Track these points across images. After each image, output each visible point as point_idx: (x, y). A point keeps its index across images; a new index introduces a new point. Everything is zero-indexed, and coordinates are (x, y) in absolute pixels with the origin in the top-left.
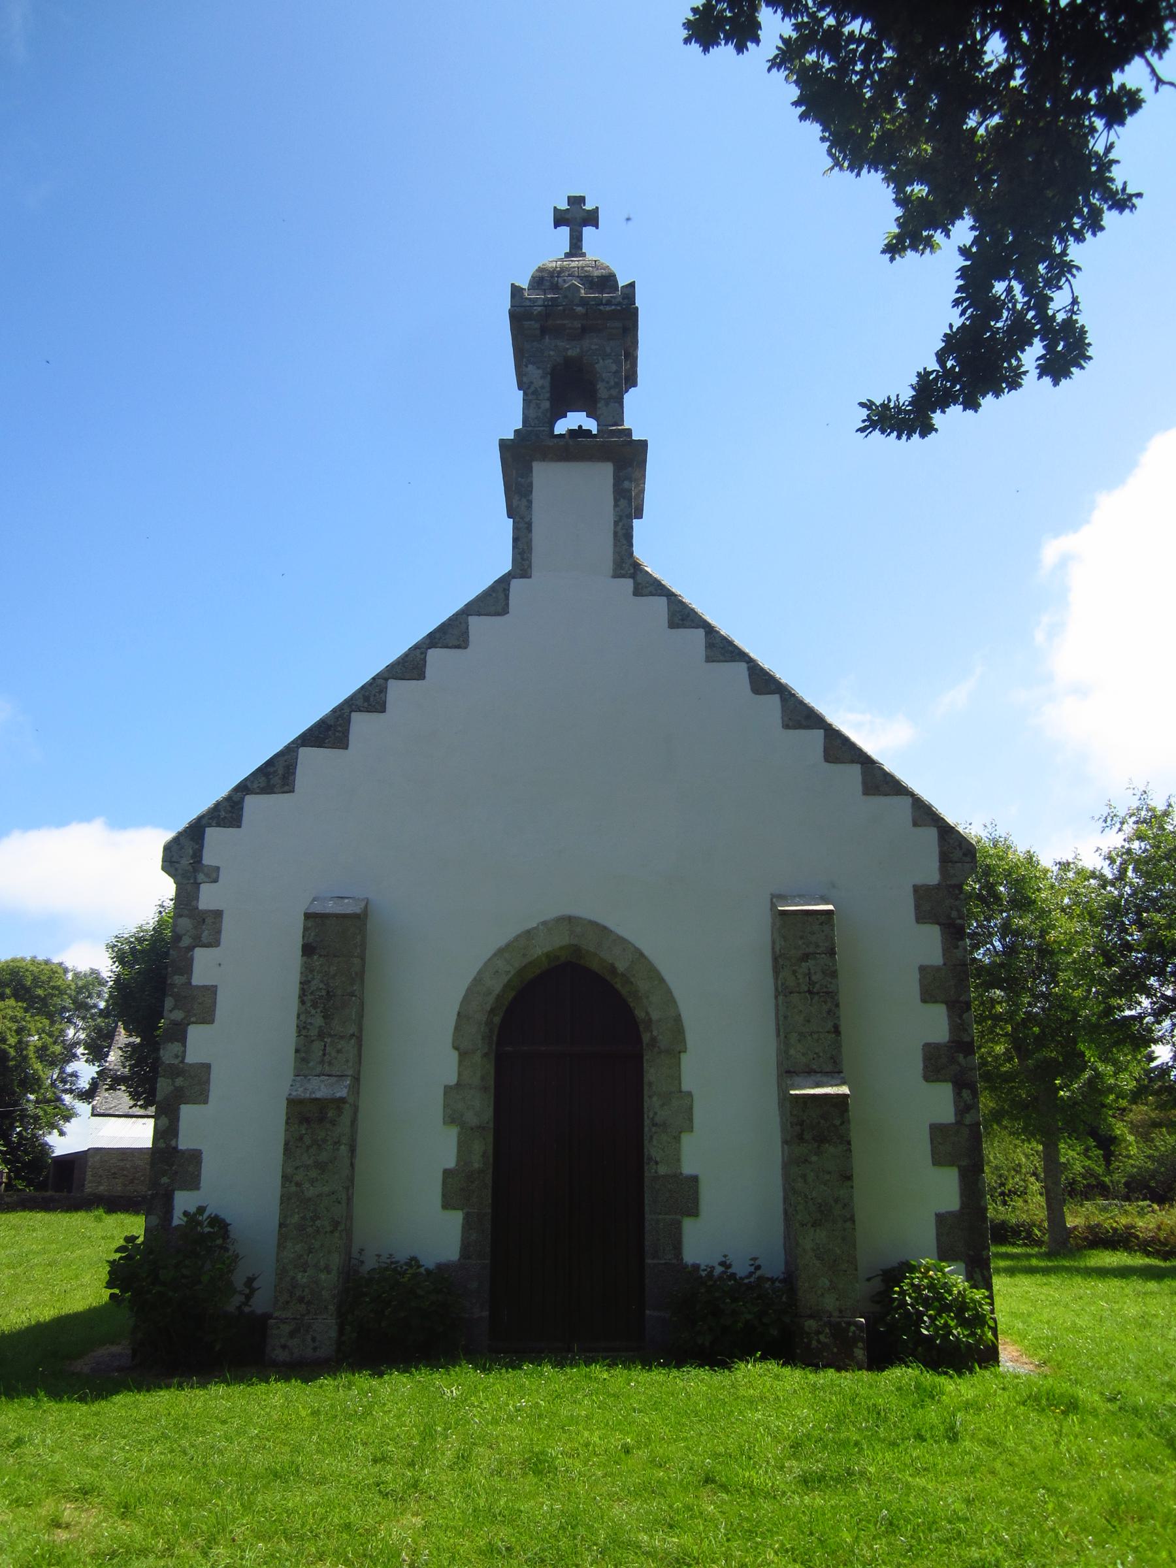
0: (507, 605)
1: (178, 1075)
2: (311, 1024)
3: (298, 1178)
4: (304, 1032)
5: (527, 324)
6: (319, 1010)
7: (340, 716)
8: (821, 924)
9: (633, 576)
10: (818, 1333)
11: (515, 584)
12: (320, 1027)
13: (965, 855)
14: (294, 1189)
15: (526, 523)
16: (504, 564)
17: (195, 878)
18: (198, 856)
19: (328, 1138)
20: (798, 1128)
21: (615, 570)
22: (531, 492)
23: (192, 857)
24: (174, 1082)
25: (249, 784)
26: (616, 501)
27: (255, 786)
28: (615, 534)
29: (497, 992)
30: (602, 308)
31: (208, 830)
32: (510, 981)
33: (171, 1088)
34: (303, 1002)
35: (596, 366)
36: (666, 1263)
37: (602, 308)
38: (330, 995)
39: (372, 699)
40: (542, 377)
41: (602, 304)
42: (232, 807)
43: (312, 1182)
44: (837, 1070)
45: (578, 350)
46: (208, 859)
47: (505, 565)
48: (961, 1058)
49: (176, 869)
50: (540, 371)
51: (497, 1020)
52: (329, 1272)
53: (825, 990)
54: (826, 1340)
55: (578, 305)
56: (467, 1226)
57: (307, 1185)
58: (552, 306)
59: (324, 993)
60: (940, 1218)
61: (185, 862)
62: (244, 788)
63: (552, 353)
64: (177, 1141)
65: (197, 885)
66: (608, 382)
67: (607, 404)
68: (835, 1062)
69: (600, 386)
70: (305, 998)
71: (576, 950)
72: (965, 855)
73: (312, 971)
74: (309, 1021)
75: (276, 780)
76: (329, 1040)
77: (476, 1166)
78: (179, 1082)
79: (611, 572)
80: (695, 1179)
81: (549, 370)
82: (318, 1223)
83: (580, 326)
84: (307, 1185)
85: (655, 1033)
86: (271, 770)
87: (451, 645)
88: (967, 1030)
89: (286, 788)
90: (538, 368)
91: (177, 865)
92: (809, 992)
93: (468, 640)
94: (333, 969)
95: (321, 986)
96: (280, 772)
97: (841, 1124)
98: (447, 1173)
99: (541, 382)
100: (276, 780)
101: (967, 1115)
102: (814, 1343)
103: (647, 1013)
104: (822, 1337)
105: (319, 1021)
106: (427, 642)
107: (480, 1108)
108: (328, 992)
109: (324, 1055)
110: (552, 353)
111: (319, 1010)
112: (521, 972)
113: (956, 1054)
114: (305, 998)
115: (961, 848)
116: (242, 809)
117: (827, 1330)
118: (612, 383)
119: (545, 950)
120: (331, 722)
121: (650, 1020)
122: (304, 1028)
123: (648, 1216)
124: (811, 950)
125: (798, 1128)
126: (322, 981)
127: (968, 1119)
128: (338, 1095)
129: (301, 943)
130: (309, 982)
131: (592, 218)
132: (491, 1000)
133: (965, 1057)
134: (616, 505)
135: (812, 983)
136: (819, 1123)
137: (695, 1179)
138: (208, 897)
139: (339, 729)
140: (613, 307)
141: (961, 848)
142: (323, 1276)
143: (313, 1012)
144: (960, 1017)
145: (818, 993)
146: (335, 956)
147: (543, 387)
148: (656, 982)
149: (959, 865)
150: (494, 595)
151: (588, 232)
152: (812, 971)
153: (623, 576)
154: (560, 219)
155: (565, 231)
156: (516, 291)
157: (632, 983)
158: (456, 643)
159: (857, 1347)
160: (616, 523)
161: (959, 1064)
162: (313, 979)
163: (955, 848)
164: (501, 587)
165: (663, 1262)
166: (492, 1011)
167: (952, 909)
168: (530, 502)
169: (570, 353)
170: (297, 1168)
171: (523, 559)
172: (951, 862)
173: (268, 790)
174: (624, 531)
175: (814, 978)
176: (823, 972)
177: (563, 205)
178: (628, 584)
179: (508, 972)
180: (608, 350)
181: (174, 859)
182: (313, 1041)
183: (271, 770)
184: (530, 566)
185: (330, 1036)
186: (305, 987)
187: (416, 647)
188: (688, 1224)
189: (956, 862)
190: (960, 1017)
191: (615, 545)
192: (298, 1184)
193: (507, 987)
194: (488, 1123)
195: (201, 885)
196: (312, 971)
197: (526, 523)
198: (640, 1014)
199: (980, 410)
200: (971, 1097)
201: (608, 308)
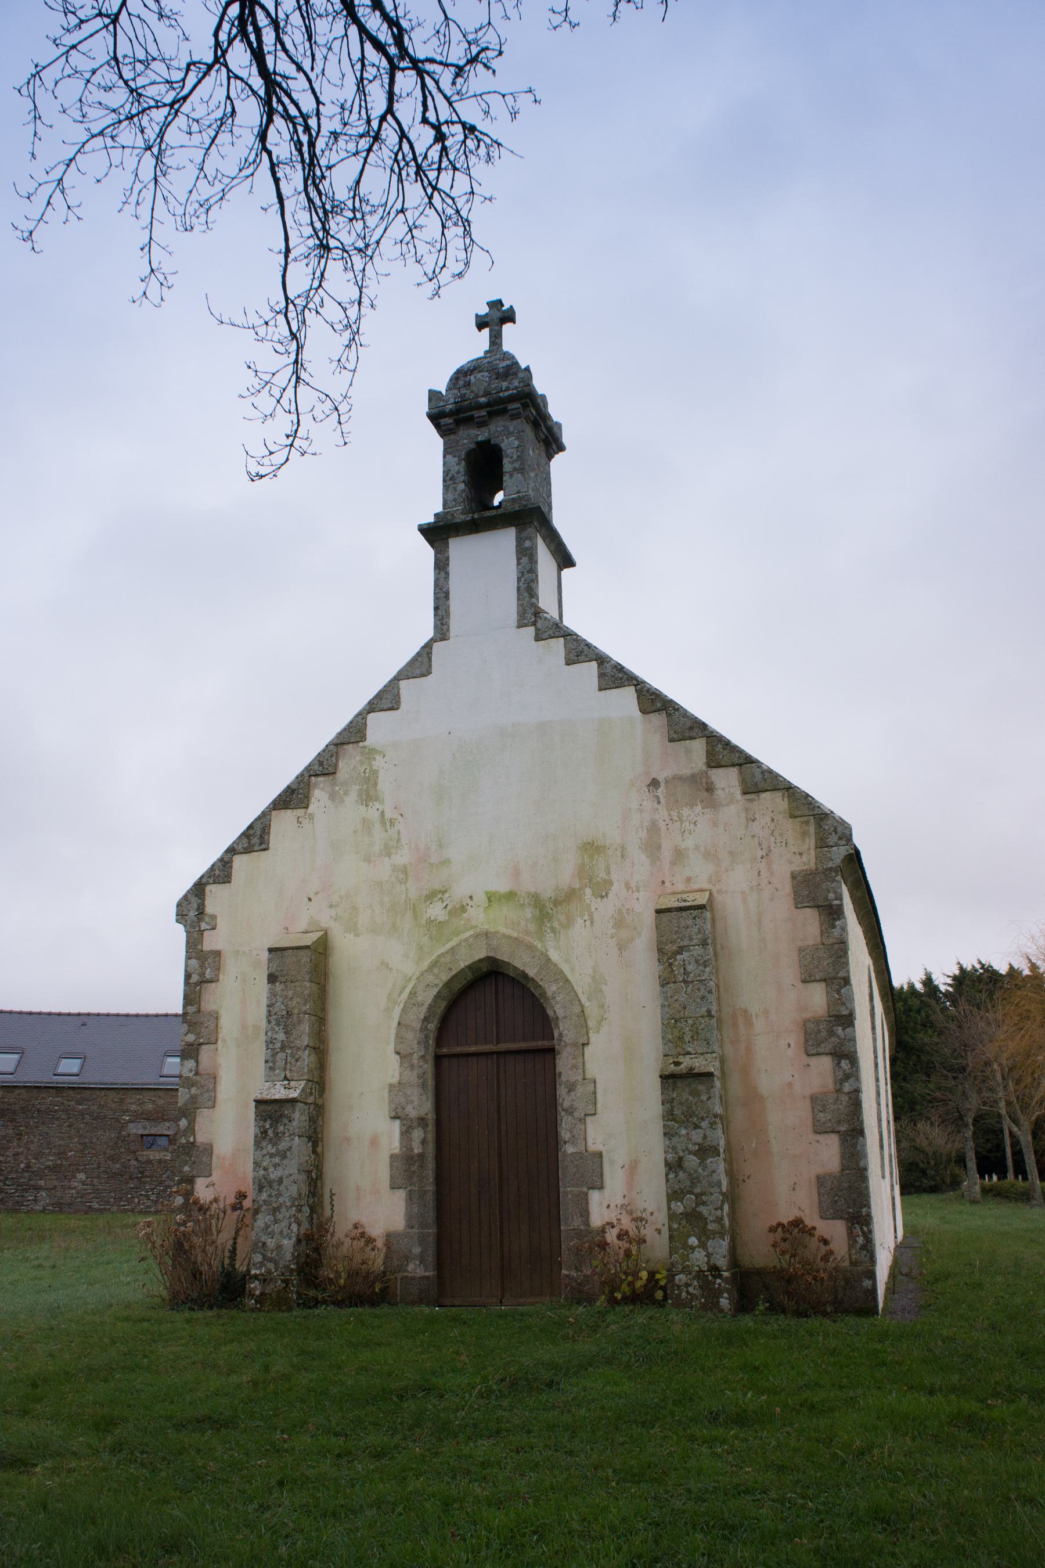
0: (430, 666)
1: (193, 1086)
2: (275, 1039)
3: (265, 1164)
4: (271, 1046)
5: (443, 421)
6: (281, 1027)
7: (301, 781)
8: (694, 918)
9: (534, 624)
10: (687, 1285)
11: (436, 646)
12: (282, 1041)
13: (840, 838)
14: (262, 1172)
15: (444, 592)
16: (428, 632)
17: (200, 926)
18: (201, 911)
19: (286, 1131)
20: (668, 1105)
21: (519, 621)
22: (448, 565)
23: (197, 910)
24: (190, 1091)
25: (235, 845)
26: (519, 559)
27: (240, 847)
28: (519, 589)
29: (428, 1003)
30: (501, 394)
31: (208, 888)
32: (439, 992)
33: (188, 1096)
34: (269, 1022)
35: (502, 445)
36: (574, 1229)
37: (501, 394)
38: (289, 1014)
39: (325, 763)
40: (458, 464)
41: (502, 391)
42: (224, 866)
43: (276, 1166)
44: (710, 1050)
45: (486, 434)
46: (209, 909)
47: (430, 633)
48: (839, 1030)
49: (186, 921)
50: (456, 459)
51: (432, 1026)
52: (290, 1239)
53: (699, 978)
54: (695, 1292)
55: (482, 396)
56: (410, 1199)
57: (271, 1169)
58: (461, 401)
59: (285, 1013)
60: (820, 1180)
61: (192, 914)
62: (232, 851)
63: (465, 441)
64: (194, 1138)
65: (201, 932)
66: (511, 457)
67: (511, 476)
68: (708, 1043)
69: (505, 461)
70: (271, 1018)
71: (491, 960)
72: (840, 838)
73: (275, 996)
74: (274, 1036)
75: (255, 840)
76: (289, 1051)
77: (416, 1151)
78: (194, 1090)
79: (516, 624)
80: (600, 1155)
81: (463, 457)
82: (281, 1200)
83: (485, 413)
84: (271, 1169)
85: (561, 1028)
86: (251, 832)
87: (385, 708)
88: (845, 1004)
89: (263, 846)
90: (455, 457)
91: (187, 918)
92: (685, 982)
93: (399, 702)
94: (290, 993)
95: (283, 1007)
96: (258, 833)
97: (707, 1100)
98: (393, 1157)
99: (456, 468)
100: (255, 840)
101: (846, 1084)
102: (684, 1294)
103: (555, 1012)
104: (691, 1289)
105: (281, 1036)
106: (368, 707)
107: (422, 1105)
108: (288, 1012)
109: (286, 1063)
110: (465, 441)
111: (281, 1027)
112: (448, 984)
113: (835, 1028)
114: (271, 1018)
115: (836, 833)
116: (231, 867)
117: (695, 1283)
118: (515, 457)
119: (467, 963)
120: (294, 787)
121: (557, 1018)
122: (271, 1043)
123: (561, 1189)
124: (686, 943)
125: (668, 1105)
126: (283, 1003)
127: (847, 1087)
128: (291, 1096)
129: (267, 973)
130: (274, 1004)
131: (509, 317)
132: (423, 1011)
133: (843, 1030)
134: (518, 564)
135: (686, 973)
136: (688, 1099)
137: (600, 1155)
138: (211, 942)
139: (301, 791)
140: (511, 392)
141: (836, 833)
142: (285, 1242)
143: (277, 1029)
144: (838, 992)
145: (692, 982)
146: (292, 982)
147: (458, 472)
148: (561, 984)
149: (834, 848)
150: (419, 659)
151: (507, 328)
152: (686, 962)
153: (526, 625)
154: (481, 323)
155: (486, 331)
156: (433, 395)
157: (540, 986)
158: (390, 706)
159: (723, 1297)
160: (519, 580)
161: (838, 1037)
162: (276, 1002)
163: (831, 834)
164: (425, 654)
165: (572, 1228)
166: (426, 1020)
167: (829, 892)
168: (447, 574)
169: (480, 439)
170: (264, 1156)
171: (442, 624)
172: (827, 847)
173: (248, 850)
174: (526, 585)
175: (689, 968)
176: (697, 961)
177: (484, 310)
178: (531, 631)
179: (436, 985)
180: (511, 429)
181: (184, 913)
182: (277, 1053)
183: (251, 832)
184: (448, 630)
185: (291, 1048)
186: (271, 1009)
187: (359, 714)
188: (594, 1197)
189: (832, 847)
190: (838, 992)
191: (519, 599)
192: (265, 1169)
193: (438, 997)
194: (427, 1114)
195: (205, 932)
196: (275, 996)
197: (444, 592)
198: (550, 1013)
199: (424, 406)
200: (849, 1066)
201: (506, 394)
